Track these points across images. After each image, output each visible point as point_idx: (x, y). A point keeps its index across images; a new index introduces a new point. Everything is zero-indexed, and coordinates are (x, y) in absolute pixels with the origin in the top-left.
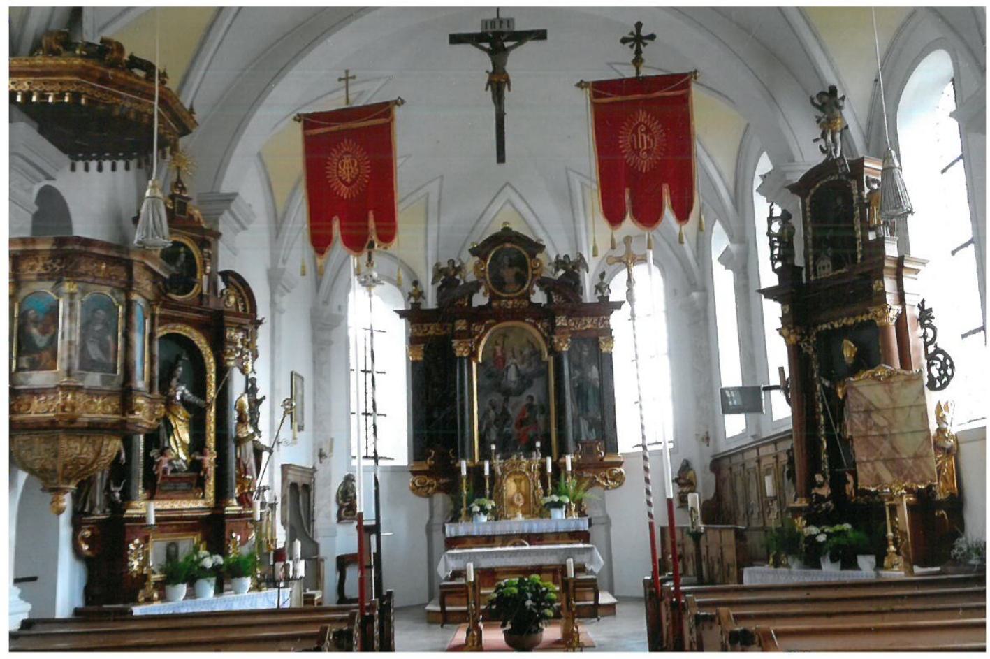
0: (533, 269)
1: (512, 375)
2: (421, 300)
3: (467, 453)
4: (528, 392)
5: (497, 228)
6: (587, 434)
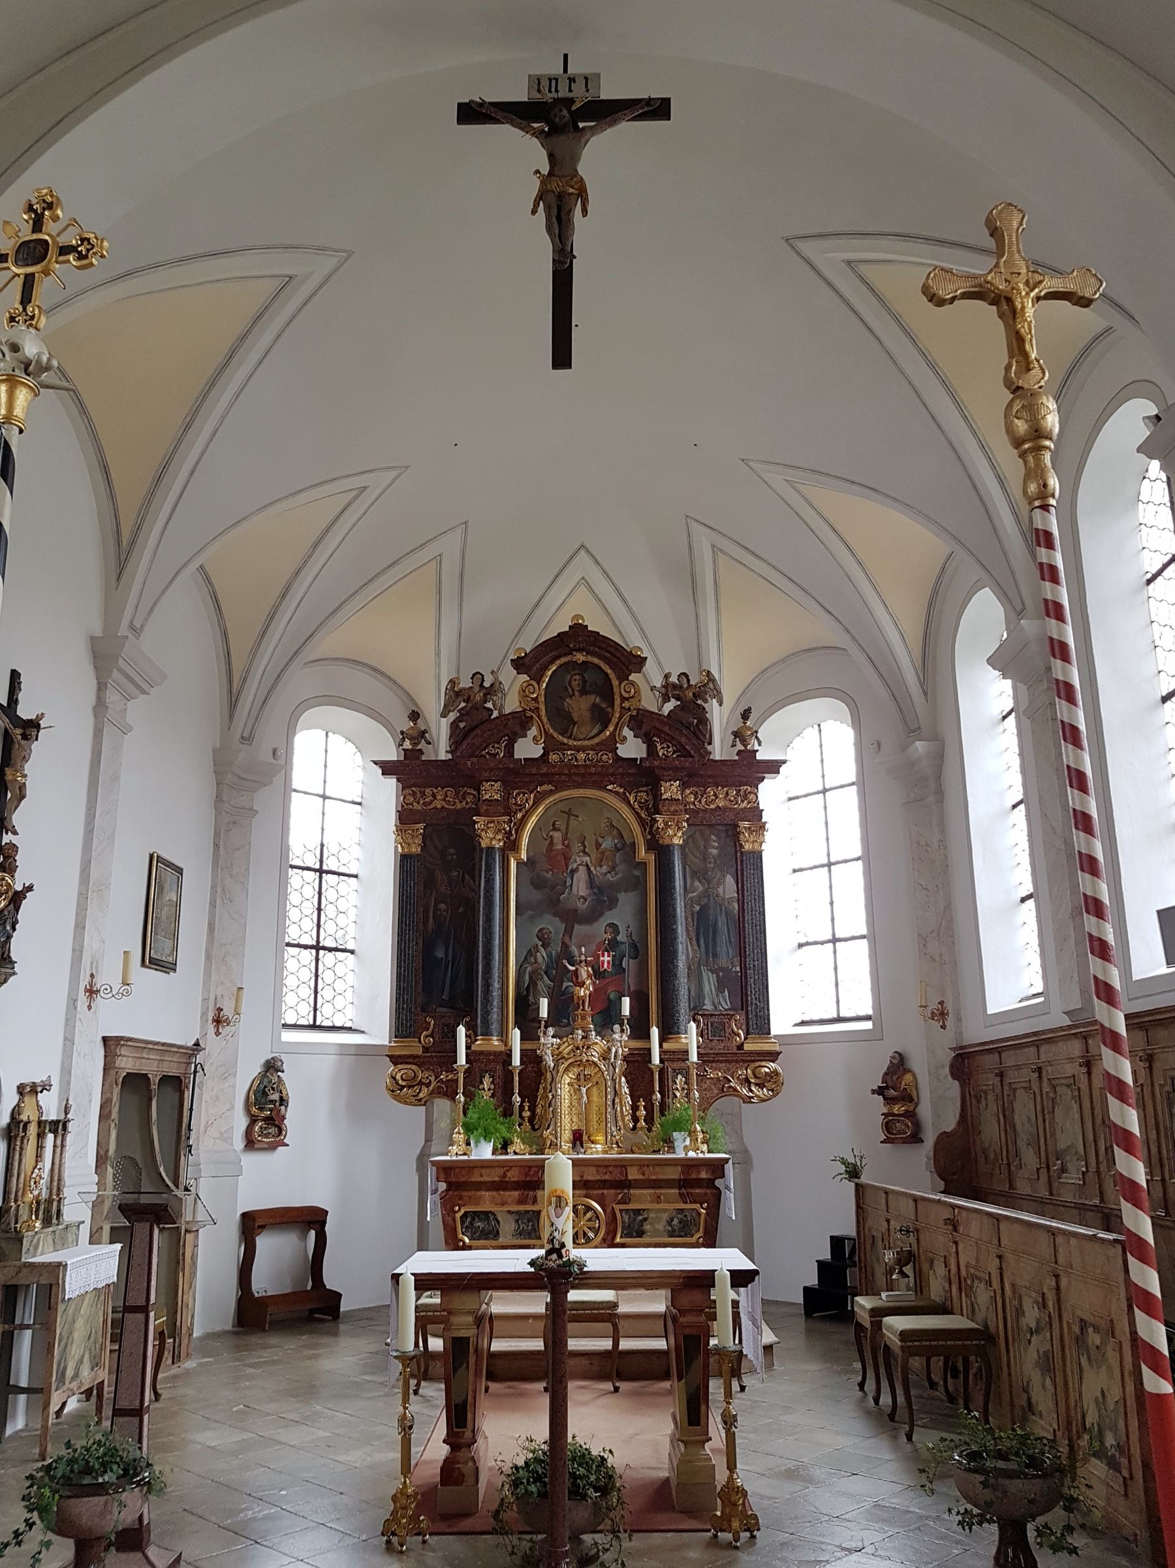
0: (623, 699)
1: (580, 886)
2: (422, 745)
3: (495, 1026)
4: (610, 917)
6: (715, 999)
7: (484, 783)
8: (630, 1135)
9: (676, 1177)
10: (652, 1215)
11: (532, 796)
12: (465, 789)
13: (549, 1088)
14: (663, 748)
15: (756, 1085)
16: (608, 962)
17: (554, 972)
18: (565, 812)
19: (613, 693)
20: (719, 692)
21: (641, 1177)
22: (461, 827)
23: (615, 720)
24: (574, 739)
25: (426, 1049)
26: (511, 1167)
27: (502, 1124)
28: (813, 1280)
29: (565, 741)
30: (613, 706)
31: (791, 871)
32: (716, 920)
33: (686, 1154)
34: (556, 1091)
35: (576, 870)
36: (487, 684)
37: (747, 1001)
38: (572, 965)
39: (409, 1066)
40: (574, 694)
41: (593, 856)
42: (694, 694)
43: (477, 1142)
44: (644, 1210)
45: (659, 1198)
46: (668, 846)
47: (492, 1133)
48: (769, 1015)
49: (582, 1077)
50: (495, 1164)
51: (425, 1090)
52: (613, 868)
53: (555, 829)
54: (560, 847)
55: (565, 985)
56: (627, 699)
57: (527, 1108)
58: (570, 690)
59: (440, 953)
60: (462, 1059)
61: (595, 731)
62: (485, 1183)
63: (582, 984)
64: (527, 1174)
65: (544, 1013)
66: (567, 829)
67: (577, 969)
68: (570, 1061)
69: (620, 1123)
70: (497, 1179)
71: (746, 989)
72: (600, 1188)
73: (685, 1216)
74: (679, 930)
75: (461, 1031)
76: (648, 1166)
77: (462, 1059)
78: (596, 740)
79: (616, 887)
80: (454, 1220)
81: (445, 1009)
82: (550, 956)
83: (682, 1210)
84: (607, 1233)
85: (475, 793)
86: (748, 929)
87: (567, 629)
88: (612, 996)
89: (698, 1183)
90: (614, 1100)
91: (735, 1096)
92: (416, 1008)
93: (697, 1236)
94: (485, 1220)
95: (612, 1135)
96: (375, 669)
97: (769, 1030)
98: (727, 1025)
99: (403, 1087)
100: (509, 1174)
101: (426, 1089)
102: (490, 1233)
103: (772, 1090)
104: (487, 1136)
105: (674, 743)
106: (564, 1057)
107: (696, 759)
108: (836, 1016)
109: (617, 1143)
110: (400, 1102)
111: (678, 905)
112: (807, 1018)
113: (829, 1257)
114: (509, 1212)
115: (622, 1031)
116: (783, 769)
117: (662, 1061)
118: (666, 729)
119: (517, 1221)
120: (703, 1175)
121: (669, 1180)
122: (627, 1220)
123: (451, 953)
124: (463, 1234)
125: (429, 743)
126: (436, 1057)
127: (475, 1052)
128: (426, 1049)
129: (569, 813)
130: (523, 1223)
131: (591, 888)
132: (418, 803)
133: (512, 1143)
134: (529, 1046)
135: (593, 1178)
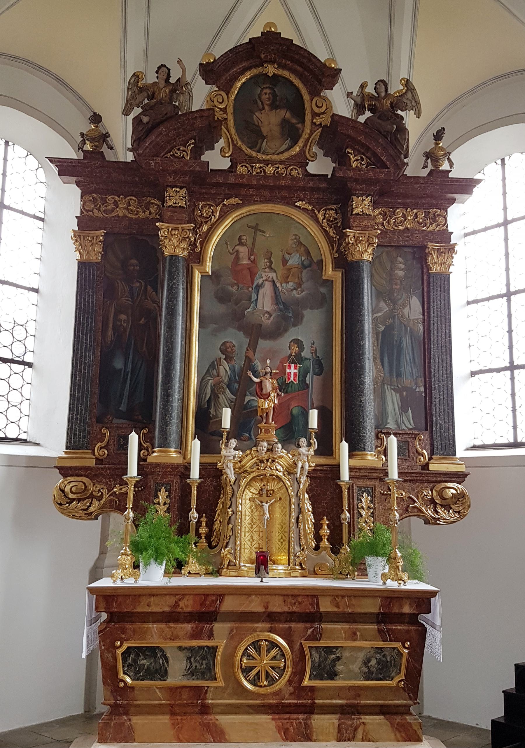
2: (104, 149)
3: (173, 437)
4: (293, 333)
5: (256, 32)
7: (169, 189)
8: (313, 555)
9: (374, 610)
10: (346, 654)
11: (219, 208)
12: (149, 199)
13: (229, 503)
14: (357, 160)
15: (442, 506)
16: (295, 374)
17: (237, 386)
18: (251, 227)
19: (304, 109)
20: (418, 103)
21: (335, 610)
22: (144, 238)
23: (305, 136)
24: (263, 154)
25: (99, 461)
26: (184, 595)
27: (176, 543)
28: (499, 712)
29: (254, 154)
30: (303, 122)
31: (465, 302)
32: (401, 342)
33: (384, 583)
34: (237, 507)
35: (262, 285)
36: (172, 80)
37: (432, 422)
38: (257, 378)
39: (79, 479)
40: (263, 108)
41: (280, 273)
42: (391, 104)
43: (147, 564)
44: (337, 648)
45: (355, 634)
46: (357, 262)
47: (164, 555)
48: (454, 435)
49: (264, 492)
50: (165, 592)
51: (96, 504)
52: (299, 285)
53: (241, 244)
54: (245, 262)
55: (247, 398)
56: (318, 115)
57: (204, 524)
58: (260, 103)
59: (118, 364)
60: (133, 470)
61: (284, 147)
62: (153, 613)
63: (267, 397)
64: (202, 604)
65: (226, 423)
66: (253, 244)
67: (261, 382)
68: (252, 475)
69: (303, 542)
70: (167, 609)
71: (431, 409)
72: (286, 621)
73: (384, 656)
74: (367, 347)
75: (134, 439)
76: (343, 597)
77: (133, 470)
78: (286, 155)
79: (302, 304)
80: (115, 657)
81: (123, 421)
82: (233, 369)
83: (381, 648)
84: (294, 674)
85: (159, 203)
86: (434, 351)
87: (260, 35)
88: (295, 411)
89: (400, 618)
90: (298, 518)
91: (418, 516)
92: (91, 419)
93: (396, 680)
94: (150, 657)
95: (295, 556)
96: (58, 79)
97: (455, 451)
98: (411, 444)
99: (72, 500)
100: (182, 604)
101: (97, 503)
102: (157, 671)
103: (459, 512)
104: (158, 557)
105: (369, 155)
106: (246, 471)
107: (392, 170)
108: (512, 441)
109: (301, 565)
110: (68, 516)
111: (366, 321)
112: (478, 443)
113: (513, 686)
114: (180, 648)
115: (309, 445)
116: (476, 190)
117: (351, 477)
118: (362, 138)
119: (189, 659)
120: (407, 609)
121: (365, 614)
122: (317, 660)
123: (130, 365)
124: (125, 673)
125: (111, 148)
126: (109, 469)
127: (151, 464)
128: (99, 461)
129: (256, 228)
130: (196, 661)
131: (277, 304)
132: (99, 210)
133: (187, 563)
134: (210, 459)
135: (279, 610)
